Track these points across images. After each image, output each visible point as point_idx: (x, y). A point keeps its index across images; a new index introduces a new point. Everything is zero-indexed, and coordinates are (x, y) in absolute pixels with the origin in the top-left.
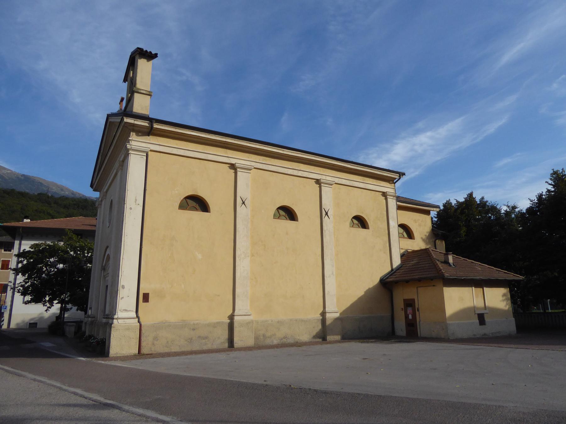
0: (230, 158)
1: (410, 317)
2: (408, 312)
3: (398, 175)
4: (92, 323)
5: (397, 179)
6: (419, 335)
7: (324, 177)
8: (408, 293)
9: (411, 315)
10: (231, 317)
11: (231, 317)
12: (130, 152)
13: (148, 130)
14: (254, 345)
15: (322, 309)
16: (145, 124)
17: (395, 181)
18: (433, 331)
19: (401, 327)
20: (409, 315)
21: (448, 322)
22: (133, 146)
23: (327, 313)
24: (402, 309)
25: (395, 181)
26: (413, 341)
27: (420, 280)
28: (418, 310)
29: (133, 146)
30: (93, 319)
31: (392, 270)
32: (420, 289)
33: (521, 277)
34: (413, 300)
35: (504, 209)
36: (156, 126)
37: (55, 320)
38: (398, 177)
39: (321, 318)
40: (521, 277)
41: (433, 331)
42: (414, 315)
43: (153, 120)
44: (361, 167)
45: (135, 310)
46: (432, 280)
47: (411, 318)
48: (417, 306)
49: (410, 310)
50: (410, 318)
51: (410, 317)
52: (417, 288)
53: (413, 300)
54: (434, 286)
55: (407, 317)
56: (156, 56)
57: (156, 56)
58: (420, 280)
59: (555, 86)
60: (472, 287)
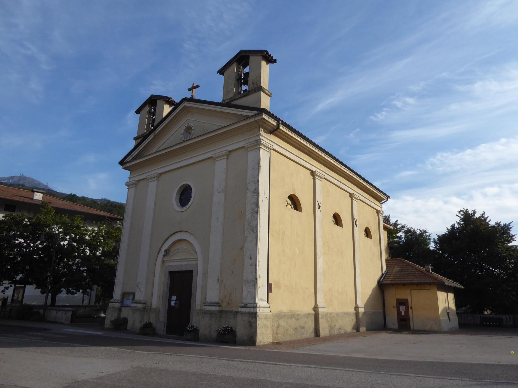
0: (312, 166)
1: (403, 313)
2: (401, 309)
3: (387, 198)
4: (144, 309)
5: (384, 201)
6: (412, 328)
7: (148, 174)
8: (403, 294)
9: (404, 312)
10: (316, 308)
11: (316, 308)
12: (261, 146)
13: (270, 128)
14: (329, 335)
15: (314, 304)
16: (273, 122)
17: (382, 202)
18: (427, 325)
19: (393, 319)
20: (402, 312)
21: (441, 319)
22: (265, 142)
23: (359, 308)
24: (394, 307)
25: (382, 202)
26: (424, 333)
27: (417, 284)
28: (411, 308)
29: (265, 142)
30: (144, 305)
31: (383, 274)
32: (413, 291)
33: (462, 287)
34: (407, 300)
35: (418, 232)
36: (281, 127)
37: (50, 304)
38: (386, 199)
39: (355, 312)
40: (462, 287)
41: (427, 325)
42: (407, 312)
43: (172, 108)
44: (373, 188)
45: (266, 300)
46: (430, 285)
47: (404, 314)
48: (410, 305)
49: (402, 308)
50: (402, 314)
51: (403, 313)
52: (411, 290)
53: (407, 300)
54: (429, 289)
55: (399, 313)
56: (275, 61)
57: (275, 61)
58: (417, 284)
59: (352, 135)
60: (445, 292)
